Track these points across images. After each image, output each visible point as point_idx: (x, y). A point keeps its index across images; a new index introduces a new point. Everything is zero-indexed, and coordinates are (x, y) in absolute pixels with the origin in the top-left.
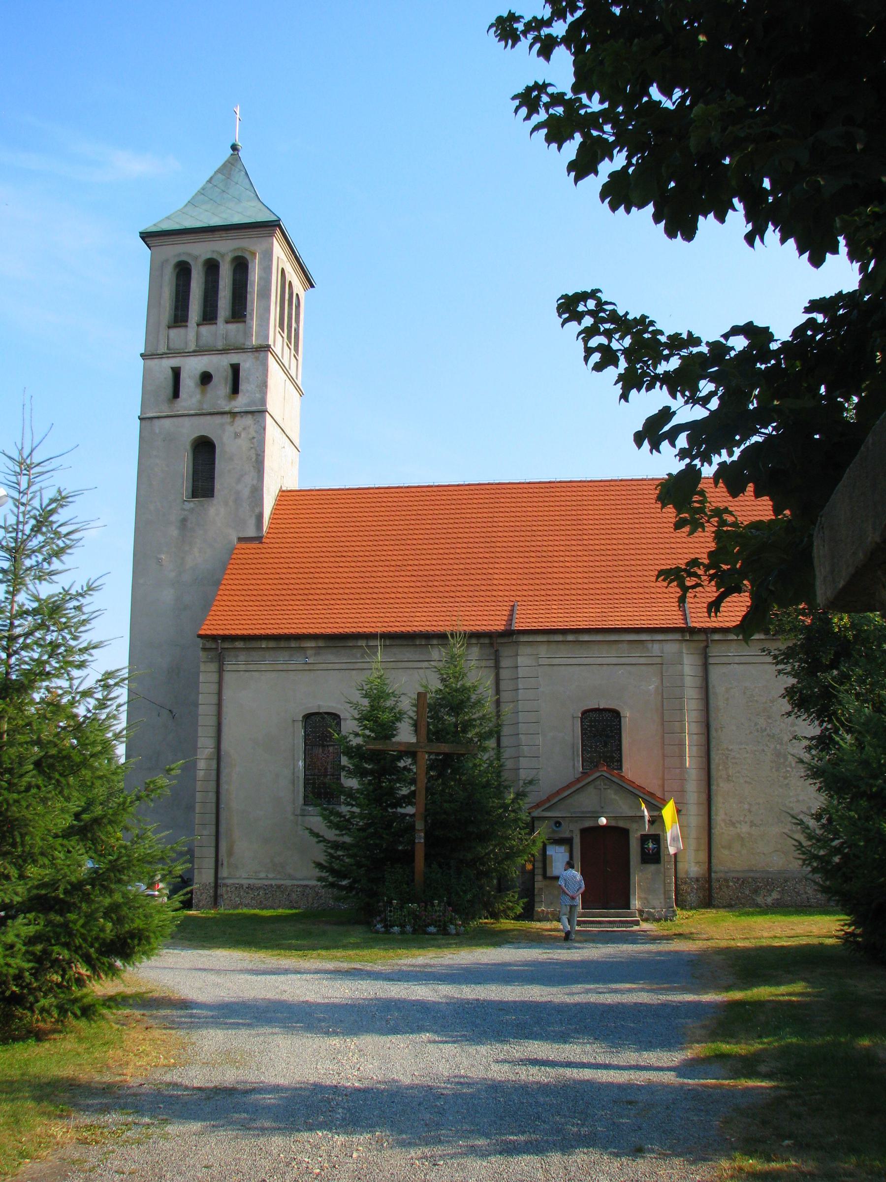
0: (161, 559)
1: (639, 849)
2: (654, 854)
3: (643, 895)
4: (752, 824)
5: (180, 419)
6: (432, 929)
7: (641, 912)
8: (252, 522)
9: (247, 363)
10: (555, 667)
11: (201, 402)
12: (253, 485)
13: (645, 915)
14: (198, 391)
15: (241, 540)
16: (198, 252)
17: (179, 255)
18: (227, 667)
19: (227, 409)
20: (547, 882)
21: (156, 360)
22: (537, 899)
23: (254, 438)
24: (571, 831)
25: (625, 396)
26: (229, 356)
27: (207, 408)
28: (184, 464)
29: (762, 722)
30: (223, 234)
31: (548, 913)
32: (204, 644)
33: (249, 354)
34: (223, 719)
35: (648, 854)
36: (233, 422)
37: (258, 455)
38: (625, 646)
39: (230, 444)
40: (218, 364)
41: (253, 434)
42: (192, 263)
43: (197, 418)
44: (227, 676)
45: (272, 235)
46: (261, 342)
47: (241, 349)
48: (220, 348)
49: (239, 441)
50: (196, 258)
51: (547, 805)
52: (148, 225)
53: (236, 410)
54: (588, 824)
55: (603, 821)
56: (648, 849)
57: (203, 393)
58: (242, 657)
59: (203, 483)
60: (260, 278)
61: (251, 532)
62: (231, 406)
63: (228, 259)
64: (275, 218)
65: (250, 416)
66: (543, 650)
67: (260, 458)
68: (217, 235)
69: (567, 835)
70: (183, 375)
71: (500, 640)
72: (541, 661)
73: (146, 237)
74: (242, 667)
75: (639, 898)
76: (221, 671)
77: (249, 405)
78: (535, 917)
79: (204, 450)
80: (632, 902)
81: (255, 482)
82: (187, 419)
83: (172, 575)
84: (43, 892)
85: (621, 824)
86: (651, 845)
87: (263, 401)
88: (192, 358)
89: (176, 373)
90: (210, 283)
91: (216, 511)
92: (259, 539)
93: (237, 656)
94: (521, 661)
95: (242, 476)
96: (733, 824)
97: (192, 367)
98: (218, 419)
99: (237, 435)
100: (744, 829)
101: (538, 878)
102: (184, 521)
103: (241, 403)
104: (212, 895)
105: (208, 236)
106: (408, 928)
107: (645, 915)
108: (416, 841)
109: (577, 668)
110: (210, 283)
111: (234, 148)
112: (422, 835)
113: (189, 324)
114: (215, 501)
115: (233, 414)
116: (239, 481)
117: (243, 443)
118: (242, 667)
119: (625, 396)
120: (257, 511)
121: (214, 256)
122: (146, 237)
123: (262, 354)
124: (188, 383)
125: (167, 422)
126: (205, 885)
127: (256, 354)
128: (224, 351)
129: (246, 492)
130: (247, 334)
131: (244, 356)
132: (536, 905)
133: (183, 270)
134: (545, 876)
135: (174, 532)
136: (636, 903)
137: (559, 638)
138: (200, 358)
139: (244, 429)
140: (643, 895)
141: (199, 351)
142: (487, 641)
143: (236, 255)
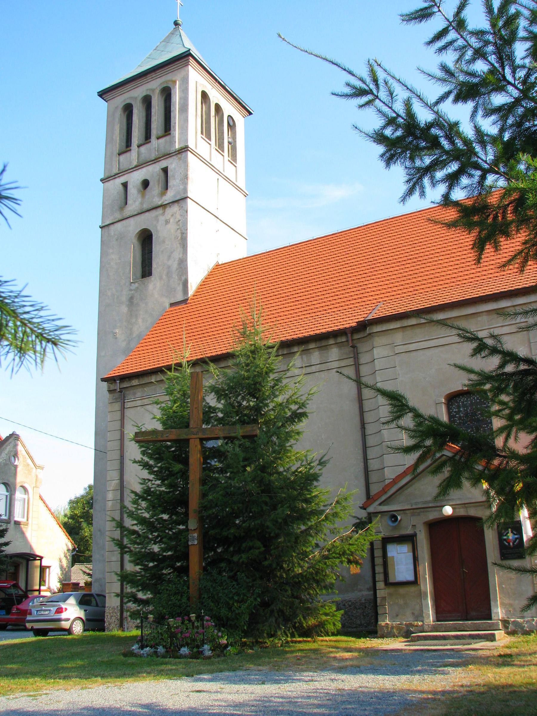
0: (116, 333)
1: (496, 542)
2: (515, 547)
3: (506, 601)
5: (127, 221)
6: (185, 650)
7: (505, 622)
8: (180, 288)
9: (172, 164)
10: (412, 354)
11: (142, 204)
12: (180, 259)
13: (511, 627)
14: (140, 196)
15: (172, 305)
17: (125, 100)
18: (127, 405)
19: (160, 203)
20: (391, 590)
21: (111, 182)
22: (380, 611)
23: (179, 221)
24: (414, 526)
26: (160, 163)
27: (146, 206)
28: (131, 252)
30: (153, 75)
31: (392, 627)
32: (109, 387)
33: (175, 157)
34: (125, 452)
35: (508, 547)
36: (164, 212)
37: (182, 233)
38: (485, 318)
39: (163, 233)
40: (151, 172)
41: (178, 217)
42: (133, 103)
43: (139, 216)
44: (128, 413)
45: (187, 65)
46: (182, 145)
47: (167, 155)
48: (153, 159)
49: (169, 226)
50: (136, 98)
51: (383, 498)
53: (166, 203)
54: (432, 516)
55: (448, 510)
56: (508, 541)
57: (143, 196)
58: (139, 393)
59: (146, 269)
60: (180, 99)
62: (163, 200)
63: (157, 91)
64: (185, 50)
65: (176, 205)
66: (398, 338)
67: (184, 235)
68: (149, 77)
69: (409, 531)
70: (130, 186)
71: (356, 336)
72: (398, 350)
73: (102, 94)
74: (139, 403)
75: (502, 604)
76: (123, 409)
77: (175, 196)
78: (379, 633)
79: (146, 239)
80: (494, 610)
81: (181, 255)
82: (132, 219)
83: (124, 344)
85: (472, 512)
86: (511, 536)
87: (185, 190)
88: (135, 172)
89: (125, 185)
90: (144, 112)
91: (154, 284)
92: (185, 301)
93: (134, 394)
94: (377, 352)
95: (172, 253)
97: (135, 178)
98: (154, 213)
99: (167, 222)
101: (380, 585)
102: (131, 299)
103: (170, 196)
104: (119, 617)
105: (143, 80)
106: (161, 649)
107: (511, 627)
108: (190, 543)
109: (436, 350)
110: (144, 112)
111: (176, 24)
112: (196, 535)
113: (132, 148)
114: (152, 278)
115: (163, 206)
116: (169, 257)
117: (172, 227)
118: (139, 403)
120: (183, 278)
121: (148, 93)
122: (102, 94)
123: (184, 154)
124: (133, 191)
125: (119, 226)
126: (114, 608)
127: (179, 156)
128: (156, 160)
129: (175, 266)
130: (173, 142)
131: (170, 160)
132: (380, 618)
133: (128, 109)
134: (388, 583)
135: (124, 309)
136: (499, 612)
137: (413, 321)
138: (140, 170)
139: (172, 215)
140: (506, 601)
141: (138, 167)
142: (344, 339)
143: (163, 87)
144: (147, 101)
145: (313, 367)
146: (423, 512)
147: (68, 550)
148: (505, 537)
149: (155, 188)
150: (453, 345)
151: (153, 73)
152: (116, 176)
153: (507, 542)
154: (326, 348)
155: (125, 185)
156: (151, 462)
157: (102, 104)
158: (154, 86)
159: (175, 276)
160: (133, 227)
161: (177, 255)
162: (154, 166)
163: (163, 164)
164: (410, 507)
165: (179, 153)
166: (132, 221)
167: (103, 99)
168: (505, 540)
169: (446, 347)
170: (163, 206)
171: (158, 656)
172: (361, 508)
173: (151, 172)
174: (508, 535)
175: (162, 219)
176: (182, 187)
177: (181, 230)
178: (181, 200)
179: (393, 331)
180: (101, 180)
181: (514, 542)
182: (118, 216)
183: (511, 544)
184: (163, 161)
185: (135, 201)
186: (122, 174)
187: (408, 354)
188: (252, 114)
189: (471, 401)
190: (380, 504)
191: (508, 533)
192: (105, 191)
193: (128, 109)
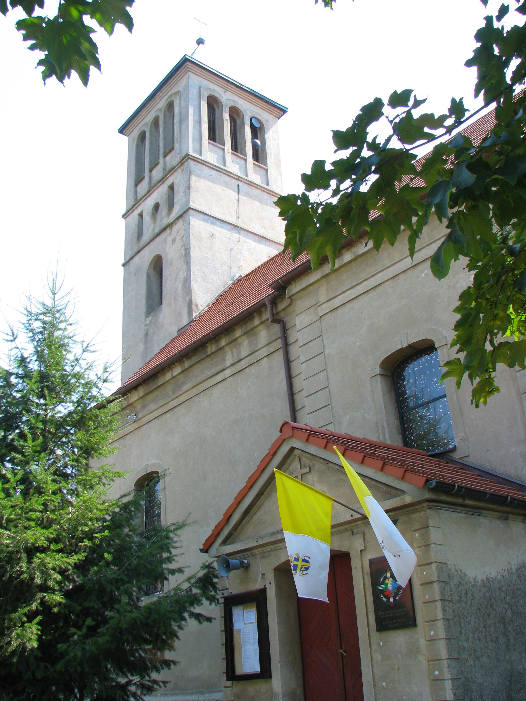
10: (340, 311)
17: (139, 129)
65: (181, 220)
70: (145, 215)
73: (122, 131)
79: (158, 265)
99: (174, 240)
109: (365, 299)
122: (122, 131)
127: (182, 167)
138: (152, 195)
145: (243, 362)
146: (275, 550)
148: (381, 587)
149: (163, 209)
150: (387, 283)
151: (159, 93)
152: (134, 208)
153: (386, 597)
154: (250, 333)
157: (124, 140)
158: (161, 103)
160: (146, 258)
161: (182, 275)
162: (162, 186)
163: (169, 182)
164: (255, 544)
165: (182, 164)
167: (124, 134)
168: (382, 591)
169: (378, 290)
172: (201, 550)
174: (387, 581)
176: (184, 199)
177: (185, 246)
179: (315, 286)
180: (123, 216)
181: (396, 594)
183: (391, 599)
184: (169, 178)
186: (138, 204)
187: (334, 313)
188: (283, 111)
189: (424, 365)
190: (225, 542)
191: (386, 578)
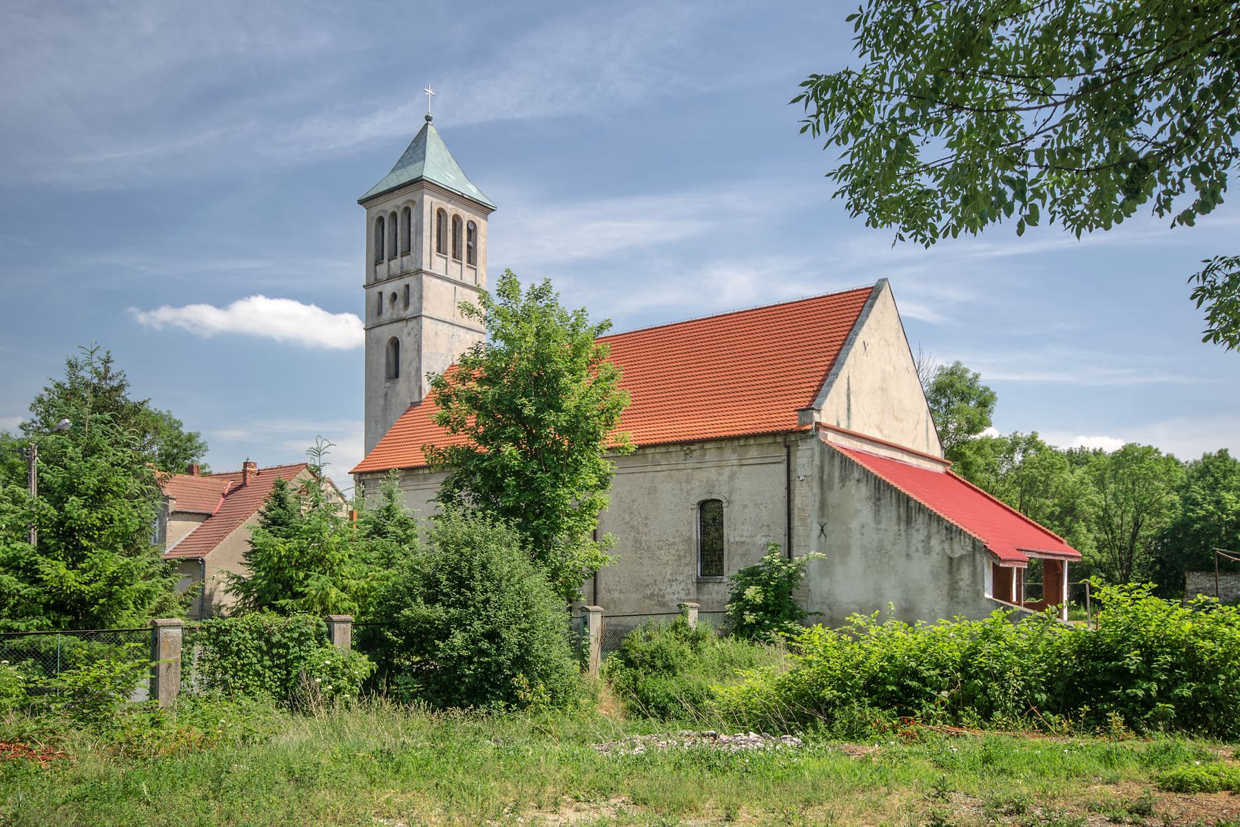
4: (621, 592)
16: (389, 206)
25: (1205, 340)
29: (627, 517)
39: (406, 343)
40: (396, 286)
47: (408, 274)
52: (363, 194)
57: (393, 307)
59: (394, 373)
61: (416, 399)
73: (361, 202)
79: (395, 344)
84: (60, 640)
96: (610, 591)
100: (616, 595)
103: (411, 311)
111: (428, 119)
115: (407, 320)
119: (1205, 340)
122: (361, 202)
141: (390, 278)
144: (394, 215)
147: (819, 411)
149: (400, 303)
155: (381, 294)
156: (1158, 189)
157: (363, 210)
158: (397, 202)
159: (413, 382)
166: (385, 328)
170: (407, 320)
171: (974, 541)
173: (396, 286)
175: (406, 330)
178: (418, 317)
182: (376, 322)
185: (388, 312)
192: (368, 297)
193: (381, 220)
